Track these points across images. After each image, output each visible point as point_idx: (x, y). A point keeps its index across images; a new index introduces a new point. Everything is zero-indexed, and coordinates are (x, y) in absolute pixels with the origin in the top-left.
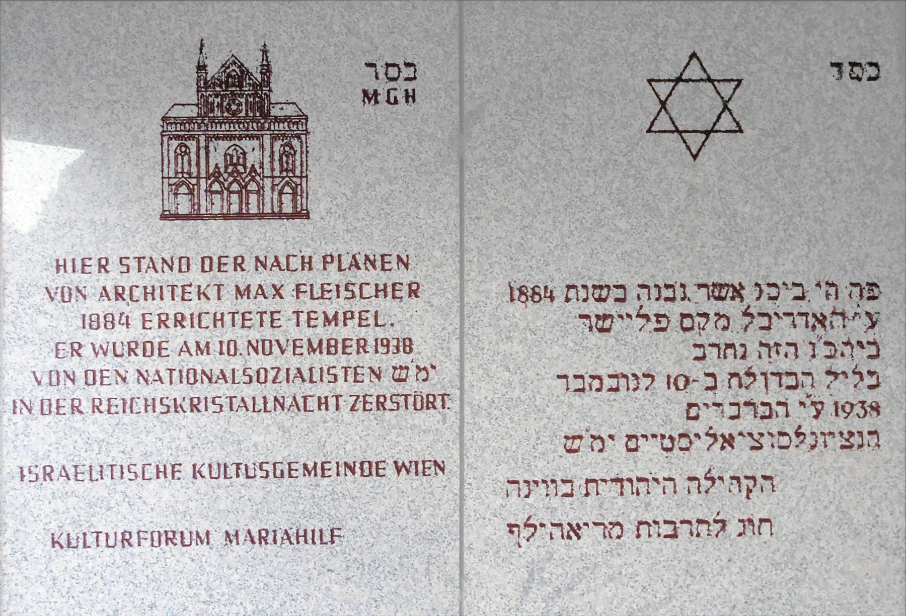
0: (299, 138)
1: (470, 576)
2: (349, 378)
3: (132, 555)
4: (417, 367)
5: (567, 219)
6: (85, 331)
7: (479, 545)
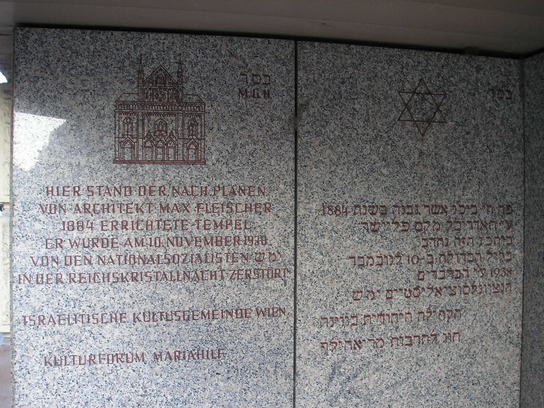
0: (200, 116)
1: (300, 373)
2: (229, 260)
3: (96, 369)
4: (270, 253)
5: (355, 168)
6: (65, 232)
7: (305, 355)
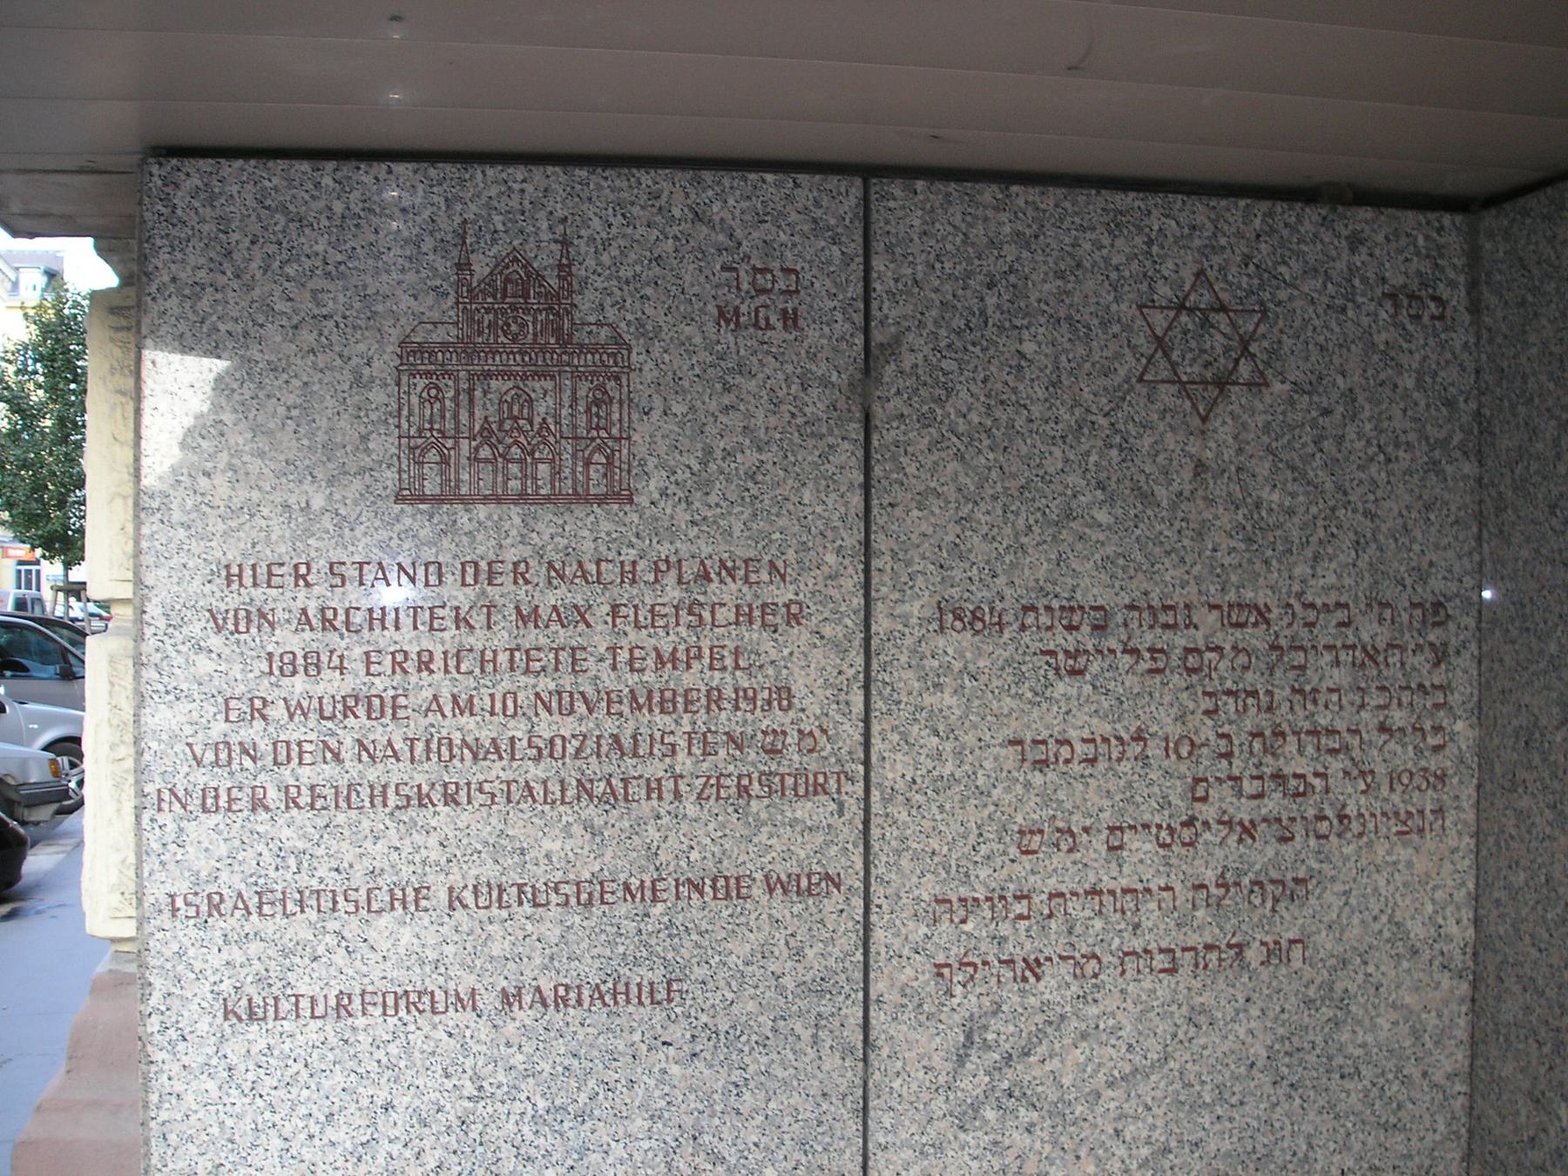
0: (617, 378)
2: (695, 750)
3: (354, 1029)
6: (273, 679)
7: (892, 997)
